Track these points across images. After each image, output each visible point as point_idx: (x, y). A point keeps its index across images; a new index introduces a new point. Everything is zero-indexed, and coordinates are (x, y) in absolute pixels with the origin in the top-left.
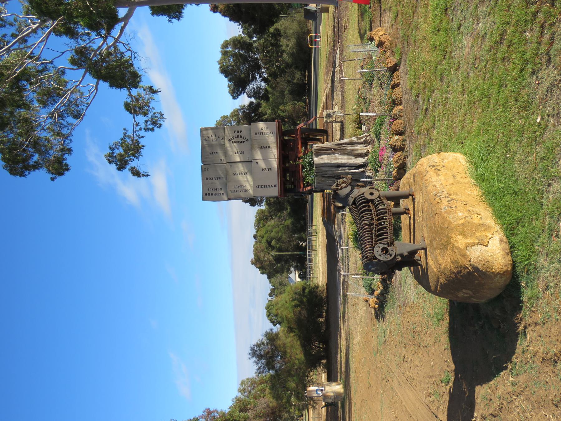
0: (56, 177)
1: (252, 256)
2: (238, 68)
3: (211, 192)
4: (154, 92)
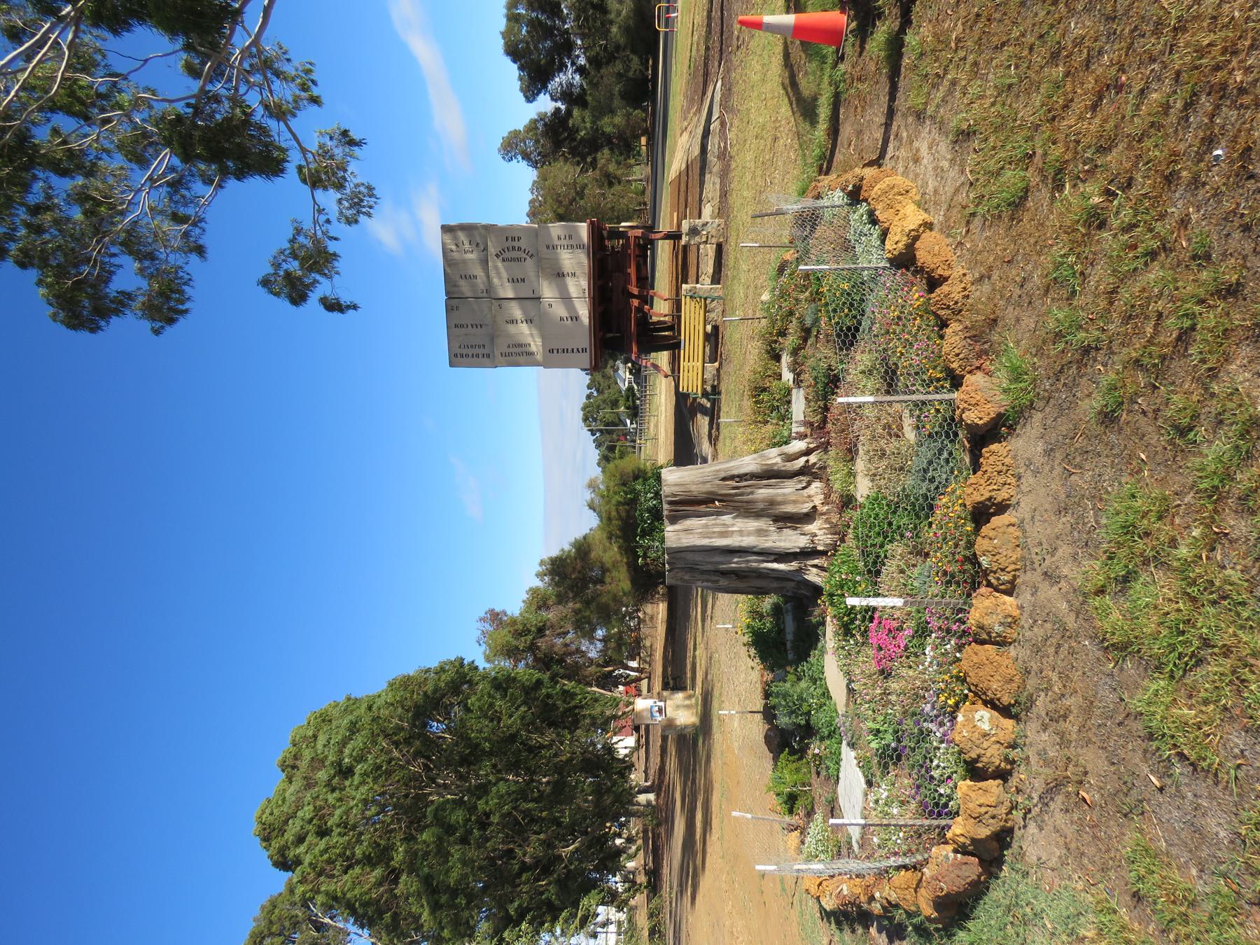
0: (162, 327)
2: (536, 47)
3: (465, 352)
4: (352, 143)
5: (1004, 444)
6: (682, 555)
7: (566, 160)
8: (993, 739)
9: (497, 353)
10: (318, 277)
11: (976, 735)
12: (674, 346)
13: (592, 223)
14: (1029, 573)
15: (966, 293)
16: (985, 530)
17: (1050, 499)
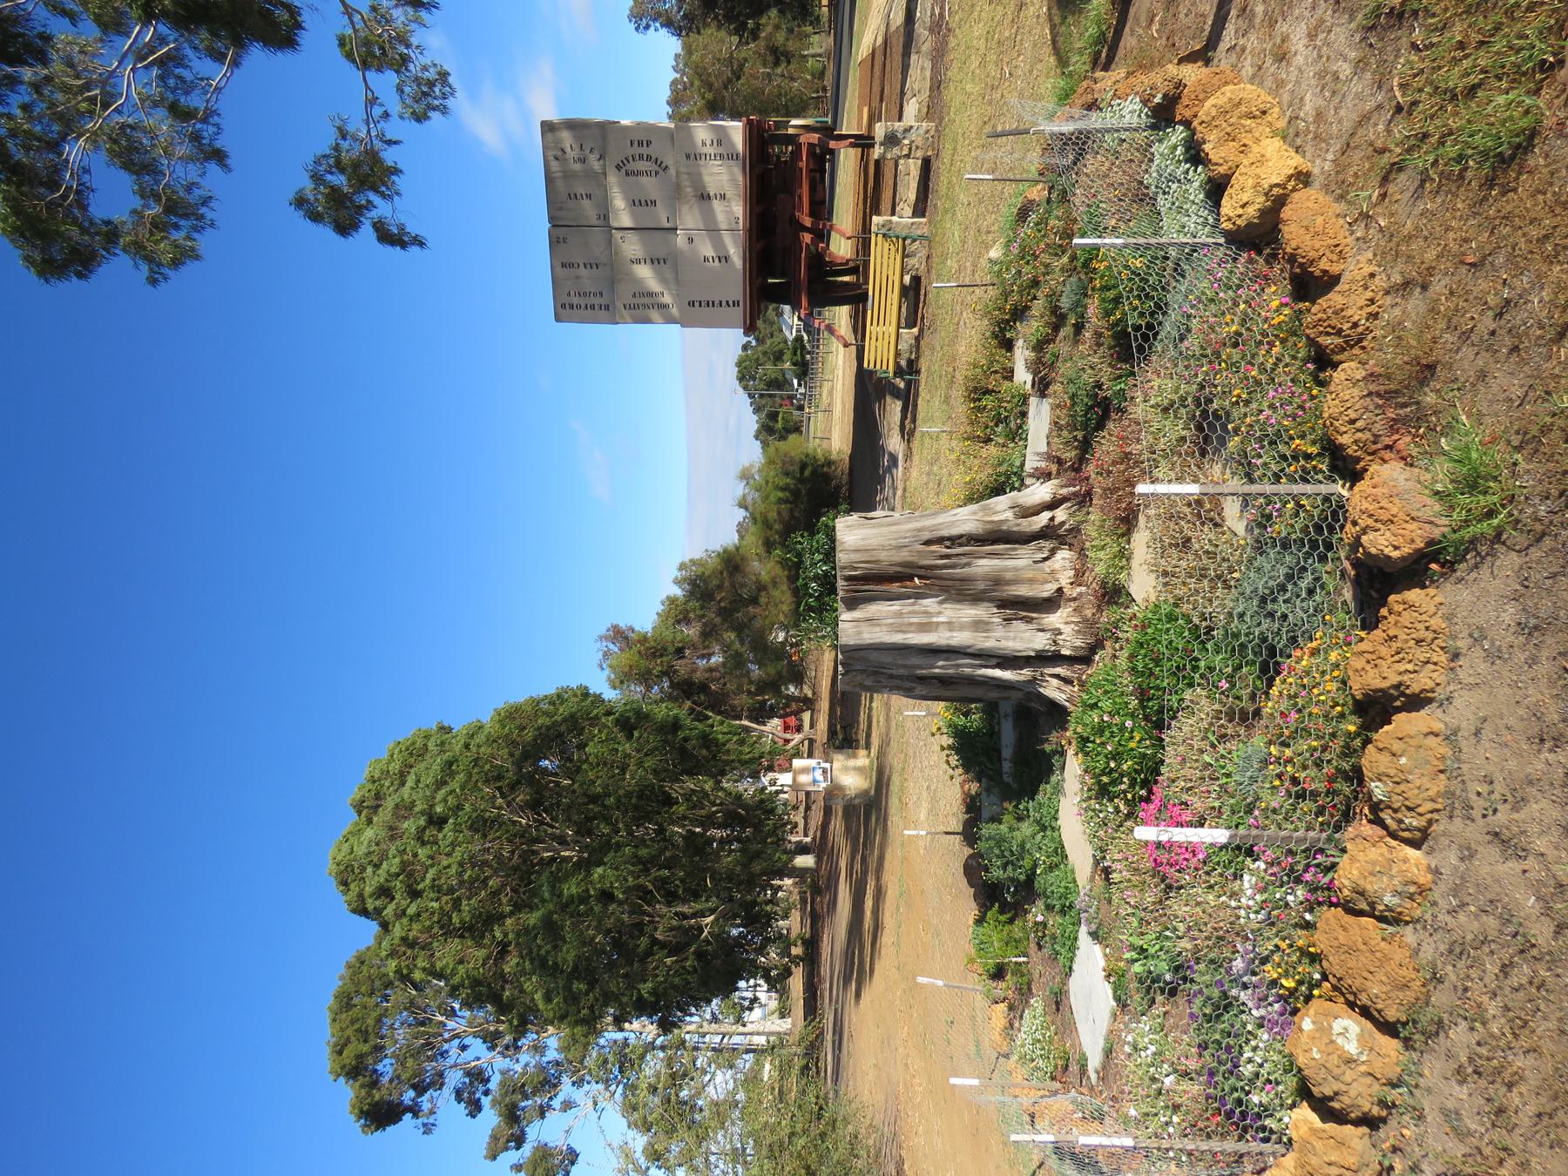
3: (575, 300)
5: (1432, 591)
6: (862, 654)
7: (719, 27)
8: (1363, 1068)
9: (619, 305)
10: (373, 197)
11: (1335, 1059)
12: (857, 298)
13: (750, 122)
14: (1458, 822)
15: (1373, 309)
16: (1384, 734)
17: (1521, 712)
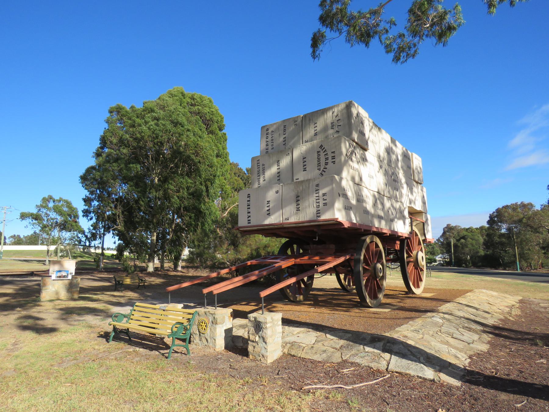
1: (453, 224)
